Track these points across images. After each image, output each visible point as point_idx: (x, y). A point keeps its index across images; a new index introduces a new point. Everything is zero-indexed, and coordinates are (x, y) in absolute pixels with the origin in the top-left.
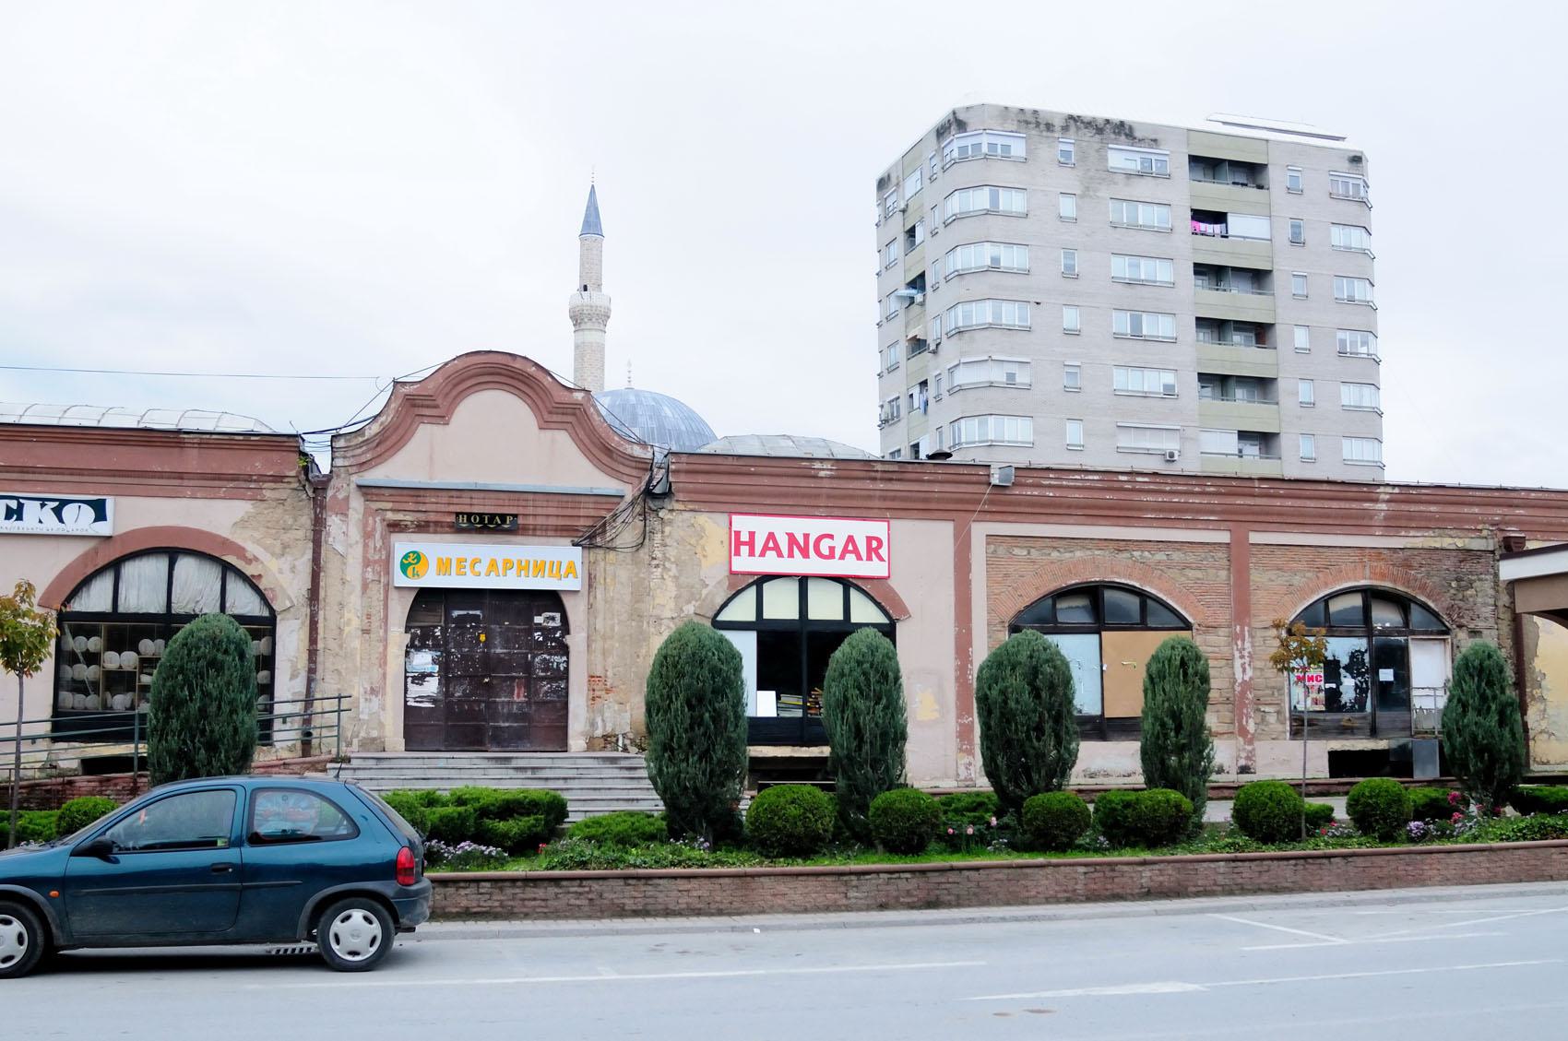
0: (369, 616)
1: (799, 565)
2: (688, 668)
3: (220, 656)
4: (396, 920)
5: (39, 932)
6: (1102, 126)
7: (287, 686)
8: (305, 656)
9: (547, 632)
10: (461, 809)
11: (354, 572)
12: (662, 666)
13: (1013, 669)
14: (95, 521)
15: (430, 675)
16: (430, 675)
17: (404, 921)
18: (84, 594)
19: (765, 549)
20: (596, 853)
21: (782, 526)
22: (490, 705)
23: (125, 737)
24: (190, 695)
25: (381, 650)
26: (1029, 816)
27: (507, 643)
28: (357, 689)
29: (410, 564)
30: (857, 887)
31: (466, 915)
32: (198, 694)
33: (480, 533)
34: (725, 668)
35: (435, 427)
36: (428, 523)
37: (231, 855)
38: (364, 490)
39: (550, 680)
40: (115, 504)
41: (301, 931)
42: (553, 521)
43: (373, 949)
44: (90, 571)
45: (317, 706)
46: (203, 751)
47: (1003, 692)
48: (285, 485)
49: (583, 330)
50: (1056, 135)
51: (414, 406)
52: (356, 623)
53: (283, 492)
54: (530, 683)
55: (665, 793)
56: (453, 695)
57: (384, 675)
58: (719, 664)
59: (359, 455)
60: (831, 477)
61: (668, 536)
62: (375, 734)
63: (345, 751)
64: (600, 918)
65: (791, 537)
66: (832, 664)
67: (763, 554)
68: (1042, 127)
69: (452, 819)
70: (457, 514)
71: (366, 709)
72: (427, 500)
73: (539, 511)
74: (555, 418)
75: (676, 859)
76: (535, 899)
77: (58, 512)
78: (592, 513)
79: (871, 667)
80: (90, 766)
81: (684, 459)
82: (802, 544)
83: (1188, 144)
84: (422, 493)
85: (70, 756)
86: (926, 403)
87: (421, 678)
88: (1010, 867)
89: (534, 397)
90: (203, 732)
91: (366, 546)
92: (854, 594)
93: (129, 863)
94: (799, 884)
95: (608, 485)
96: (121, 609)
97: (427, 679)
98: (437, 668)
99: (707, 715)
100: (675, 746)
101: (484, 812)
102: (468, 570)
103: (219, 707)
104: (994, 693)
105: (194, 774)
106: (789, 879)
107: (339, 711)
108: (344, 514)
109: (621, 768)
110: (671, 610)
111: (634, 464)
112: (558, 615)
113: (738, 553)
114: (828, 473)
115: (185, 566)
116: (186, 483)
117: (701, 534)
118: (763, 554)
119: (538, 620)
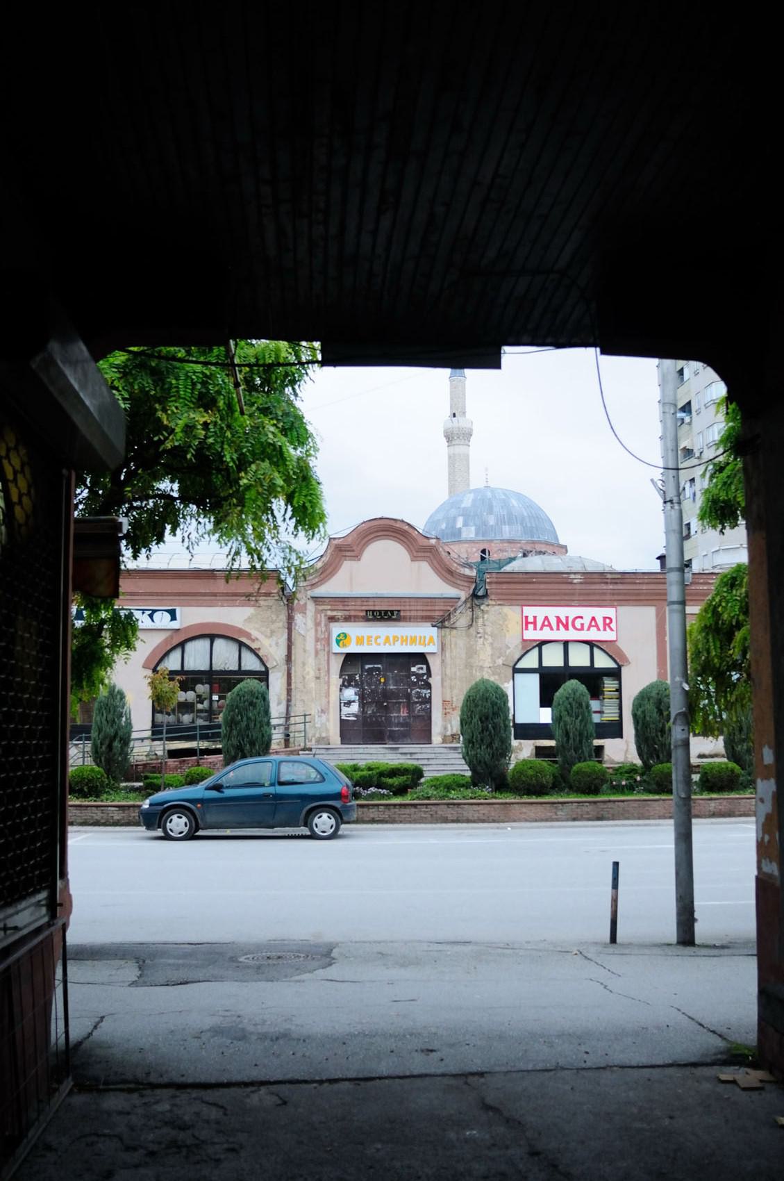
0: (319, 670)
1: (563, 635)
2: (480, 702)
3: (254, 700)
4: (341, 818)
5: (193, 822)
7: (276, 711)
8: (285, 693)
9: (418, 676)
10: (370, 772)
11: (310, 645)
12: (467, 701)
13: (649, 700)
14: (172, 620)
15: (354, 701)
16: (354, 701)
17: (345, 818)
18: (166, 660)
19: (543, 625)
20: (435, 793)
21: (552, 612)
22: (388, 719)
23: (192, 738)
24: (242, 719)
25: (326, 688)
26: (654, 775)
27: (396, 683)
28: (314, 710)
29: (341, 640)
30: (561, 809)
31: (373, 821)
32: (245, 719)
33: (380, 621)
34: (499, 702)
35: (353, 562)
36: (350, 617)
37: (271, 790)
38: (315, 599)
39: (421, 703)
40: (181, 611)
41: (301, 822)
42: (420, 614)
43: (332, 830)
44: (170, 647)
45: (292, 720)
46: (248, 745)
47: (643, 712)
48: (272, 598)
49: (454, 445)
51: (341, 551)
52: (312, 674)
53: (271, 601)
54: (410, 705)
55: (470, 764)
56: (367, 712)
57: (328, 702)
58: (496, 700)
59: (311, 580)
60: (581, 583)
61: (487, 620)
62: (324, 735)
63: (309, 745)
64: (435, 823)
65: (558, 618)
66: (555, 698)
67: (541, 629)
69: (366, 777)
70: (367, 611)
71: (319, 722)
72: (349, 604)
73: (413, 608)
74: (420, 554)
75: (473, 796)
76: (405, 814)
77: (151, 616)
78: (442, 608)
79: (574, 700)
80: (173, 754)
81: (494, 575)
82: (561, 625)
84: (346, 600)
85: (160, 748)
86: (694, 494)
87: (348, 703)
88: (639, 800)
89: (408, 543)
90: (248, 736)
91: (316, 631)
92: (596, 651)
93: (228, 793)
94: (533, 808)
95: (451, 591)
96: (186, 669)
97: (352, 704)
98: (357, 697)
99: (490, 725)
100: (474, 741)
101: (382, 774)
102: (373, 642)
103: (255, 725)
104: (639, 713)
105: (244, 757)
106: (527, 805)
107: (305, 723)
108: (304, 613)
109: (401, 753)
110: (489, 662)
111: (466, 579)
112: (424, 667)
113: (527, 629)
114: (579, 580)
115: (219, 643)
116: (218, 598)
117: (505, 618)
118: (541, 629)
119: (413, 669)
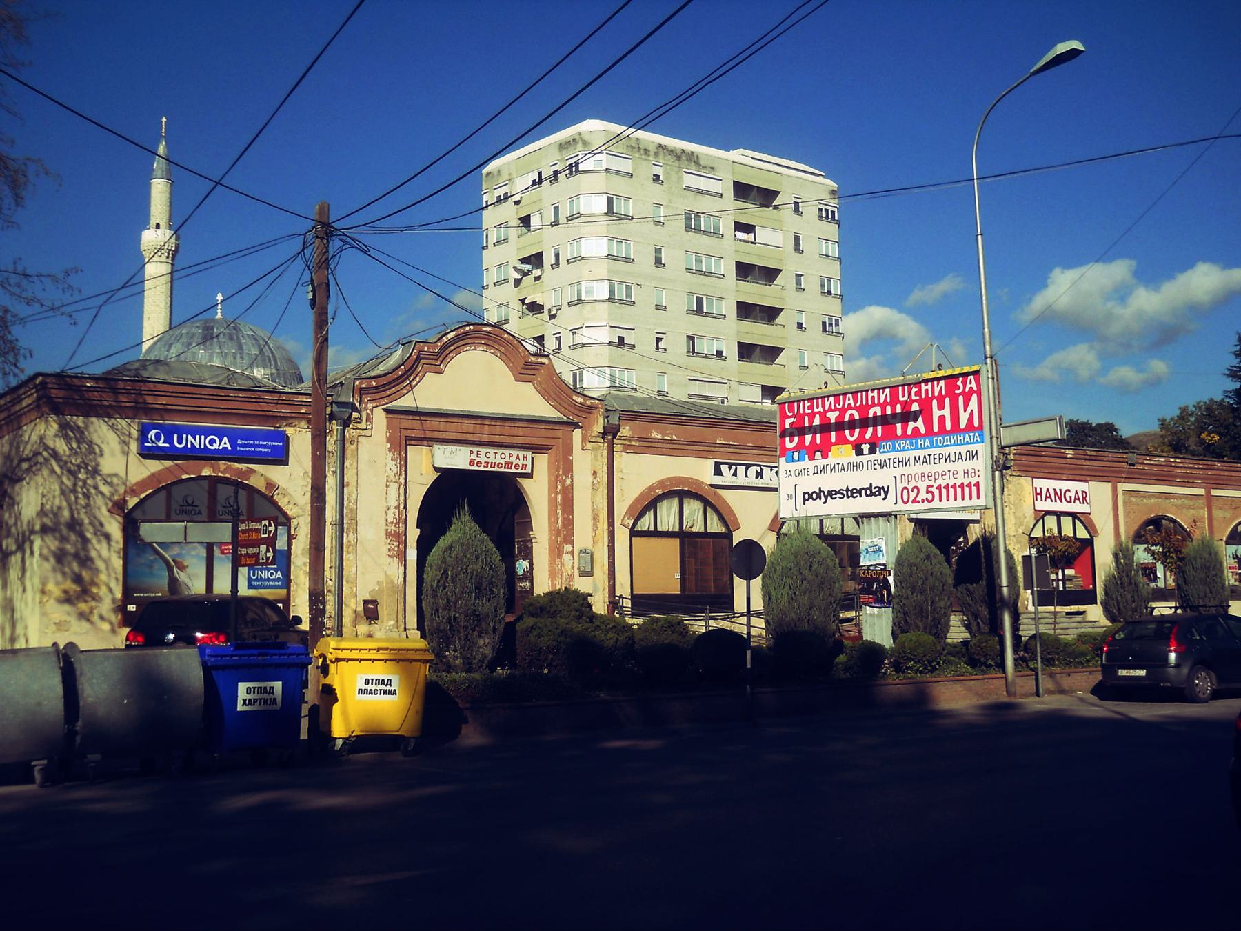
6: (680, 154)
50: (651, 159)
68: (642, 151)
83: (733, 173)
113: (1037, 500)
